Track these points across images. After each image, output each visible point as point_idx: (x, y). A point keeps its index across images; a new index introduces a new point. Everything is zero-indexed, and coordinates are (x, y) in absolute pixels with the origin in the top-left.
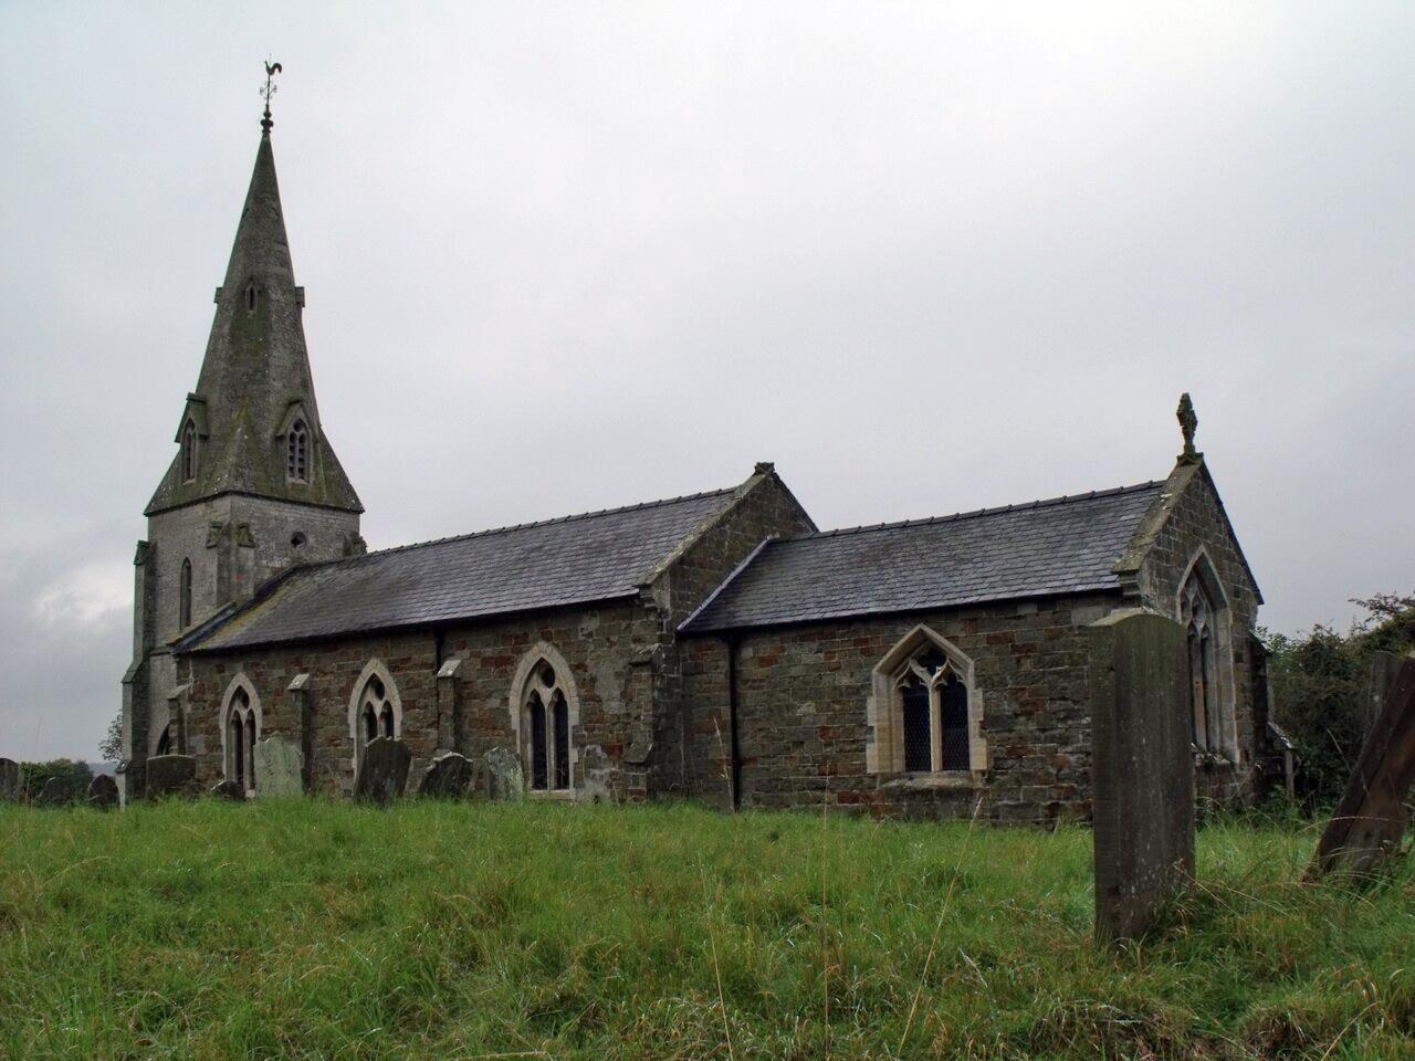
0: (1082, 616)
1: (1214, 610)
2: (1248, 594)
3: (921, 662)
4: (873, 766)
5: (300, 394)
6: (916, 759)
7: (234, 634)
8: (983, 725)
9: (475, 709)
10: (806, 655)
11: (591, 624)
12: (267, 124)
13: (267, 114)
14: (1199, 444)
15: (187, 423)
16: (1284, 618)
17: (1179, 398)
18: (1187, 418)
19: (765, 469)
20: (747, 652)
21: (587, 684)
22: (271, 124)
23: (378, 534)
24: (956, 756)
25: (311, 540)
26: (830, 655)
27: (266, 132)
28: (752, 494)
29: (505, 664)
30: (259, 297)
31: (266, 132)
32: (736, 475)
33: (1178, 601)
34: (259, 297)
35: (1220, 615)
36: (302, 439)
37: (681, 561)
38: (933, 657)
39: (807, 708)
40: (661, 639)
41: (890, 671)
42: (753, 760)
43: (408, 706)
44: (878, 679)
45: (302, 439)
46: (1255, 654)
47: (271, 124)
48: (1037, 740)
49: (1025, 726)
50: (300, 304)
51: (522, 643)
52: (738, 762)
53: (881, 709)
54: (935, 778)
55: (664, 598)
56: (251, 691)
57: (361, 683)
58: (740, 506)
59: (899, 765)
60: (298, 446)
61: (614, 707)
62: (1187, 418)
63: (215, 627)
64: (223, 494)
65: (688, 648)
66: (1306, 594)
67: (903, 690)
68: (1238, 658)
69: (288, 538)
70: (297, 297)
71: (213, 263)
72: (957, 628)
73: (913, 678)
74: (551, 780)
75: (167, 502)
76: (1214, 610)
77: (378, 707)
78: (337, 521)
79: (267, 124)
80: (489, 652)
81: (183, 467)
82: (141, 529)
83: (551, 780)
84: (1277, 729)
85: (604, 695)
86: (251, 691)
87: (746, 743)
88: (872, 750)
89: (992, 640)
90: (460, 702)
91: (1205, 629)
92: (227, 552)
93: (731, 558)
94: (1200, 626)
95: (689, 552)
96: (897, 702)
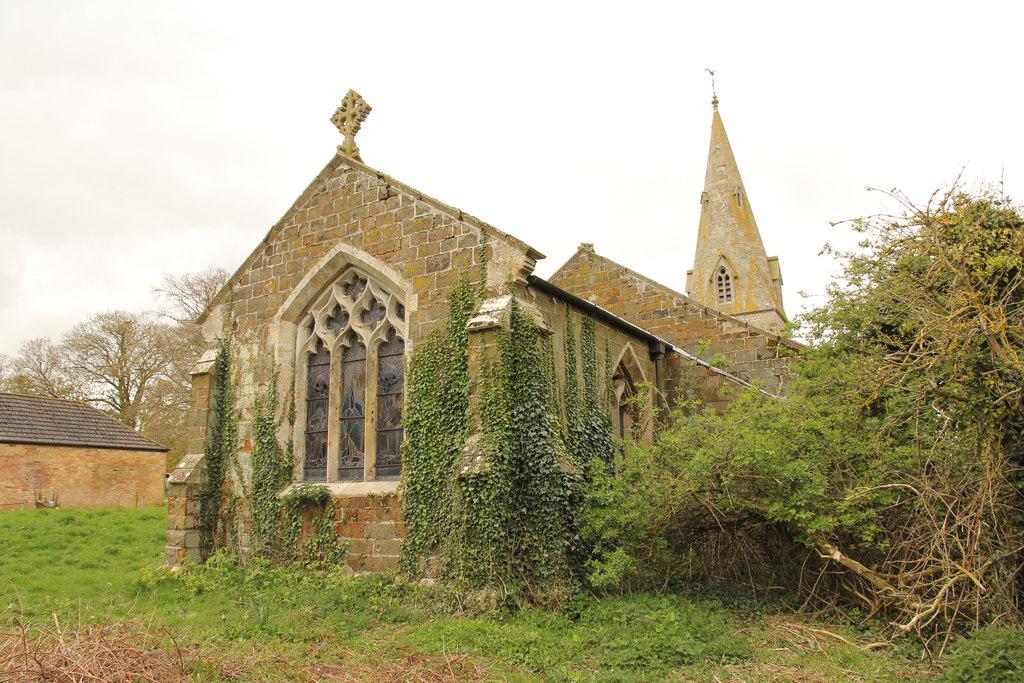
12: (715, 102)
13: (715, 98)
22: (717, 102)
27: (716, 107)
31: (716, 107)
36: (727, 278)
47: (717, 102)
60: (724, 282)
79: (715, 102)
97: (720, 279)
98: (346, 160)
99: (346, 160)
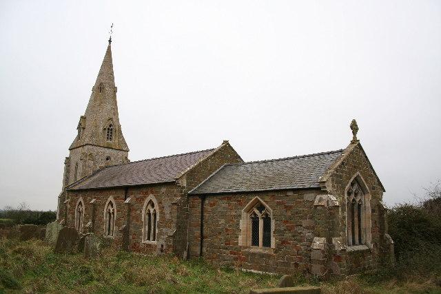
0: (308, 196)
1: (364, 194)
2: (379, 188)
3: (258, 209)
4: (240, 244)
5: (112, 116)
6: (255, 242)
7: (83, 185)
8: (274, 233)
9: (133, 214)
10: (223, 204)
11: (163, 190)
12: (110, 41)
14: (359, 136)
15: (80, 124)
16: (390, 201)
17: (350, 123)
18: (354, 127)
19: (226, 142)
20: (207, 202)
21: (162, 208)
23: (133, 157)
24: (267, 243)
25: (112, 159)
26: (230, 205)
28: (220, 150)
29: (141, 200)
30: (105, 89)
32: (216, 144)
33: (346, 192)
34: (105, 89)
35: (366, 195)
36: (111, 130)
37: (192, 171)
38: (261, 208)
39: (222, 221)
40: (182, 196)
41: (248, 211)
42: (207, 237)
43: (118, 211)
44: (244, 214)
45: (111, 130)
46: (379, 209)
48: (291, 240)
49: (288, 235)
50: (115, 91)
51: (147, 194)
52: (202, 237)
53: (245, 223)
54: (259, 249)
55: (184, 183)
56: (82, 202)
57: (107, 203)
58: (214, 154)
59: (250, 243)
61: (168, 216)
62: (354, 127)
63: (74, 185)
64: (86, 145)
65: (191, 199)
66: (402, 187)
67: (252, 218)
68: (373, 211)
69: (105, 158)
70: (115, 90)
71: (92, 81)
72: (267, 198)
73: (255, 214)
74: (152, 238)
75: (75, 146)
76: (364, 194)
77: (111, 211)
78: (120, 153)
79: (110, 41)
80: (138, 196)
81: (79, 137)
82: (68, 154)
83: (152, 238)
84: (388, 236)
85: (166, 212)
86: (82, 202)
87: (204, 232)
88: (240, 238)
89: (279, 204)
90: (130, 210)
91: (360, 201)
92: (85, 161)
93: (210, 170)
94: (357, 200)
95: (194, 168)
96: (250, 222)
97: (108, 129)
98: (355, 141)
99: (355, 141)
